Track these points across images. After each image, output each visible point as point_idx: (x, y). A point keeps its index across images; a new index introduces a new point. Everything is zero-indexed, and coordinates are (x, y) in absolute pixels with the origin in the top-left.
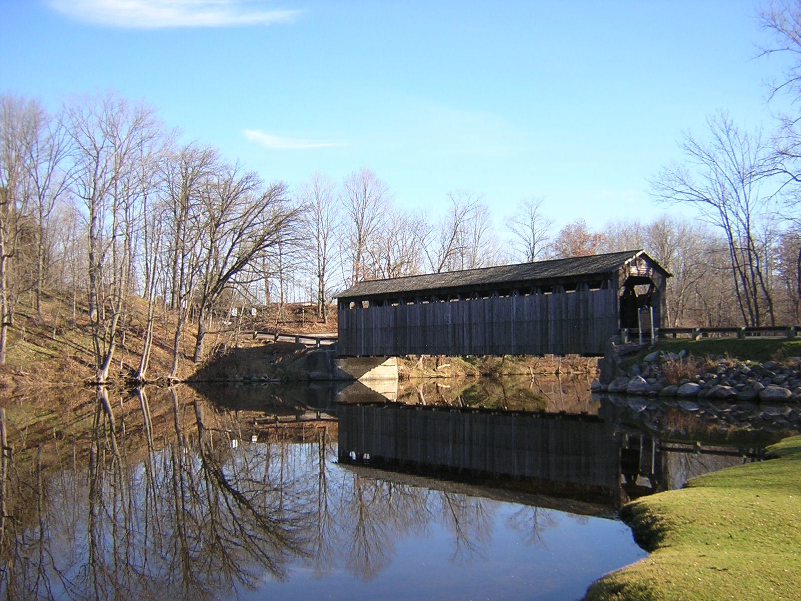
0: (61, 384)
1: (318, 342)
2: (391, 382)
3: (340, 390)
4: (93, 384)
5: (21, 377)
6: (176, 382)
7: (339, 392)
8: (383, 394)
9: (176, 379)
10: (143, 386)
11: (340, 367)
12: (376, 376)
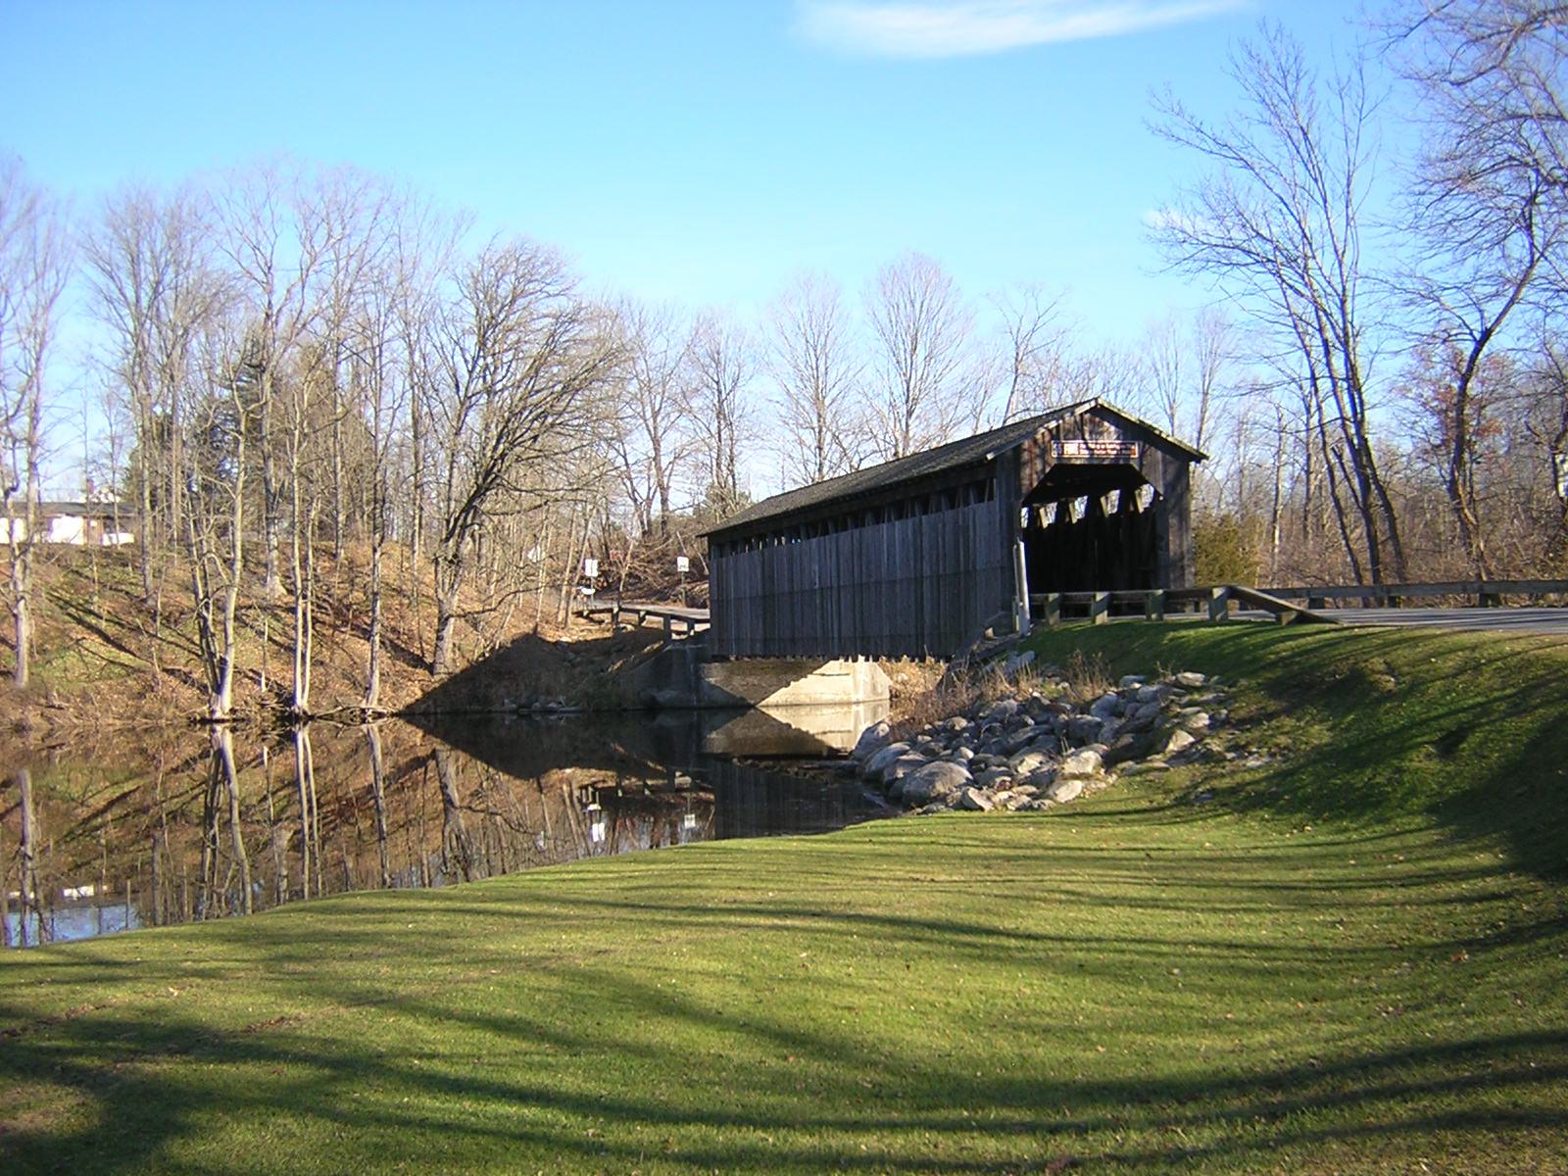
0: (140, 722)
1: (691, 627)
2: (838, 709)
3: (714, 728)
4: (204, 721)
5: (58, 712)
6: (380, 715)
7: (710, 732)
8: (819, 737)
9: (380, 709)
10: (305, 724)
11: (712, 680)
12: (803, 699)
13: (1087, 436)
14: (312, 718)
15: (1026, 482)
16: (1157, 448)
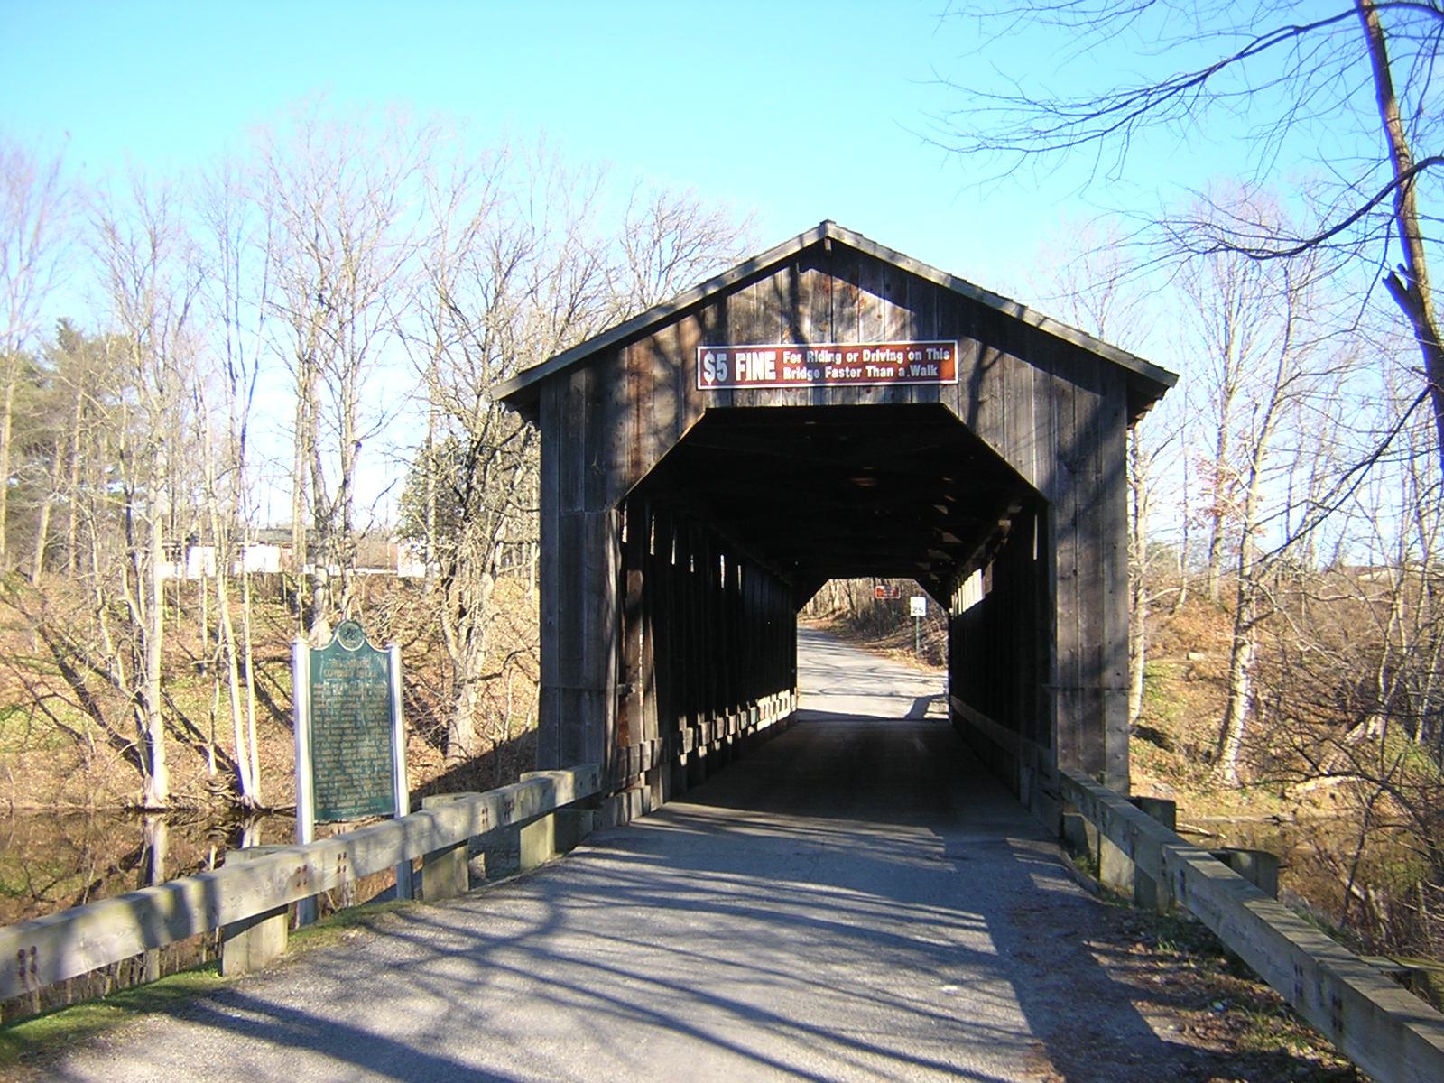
13: (807, 326)
14: (267, 811)
15: (624, 459)
16: (1021, 355)
